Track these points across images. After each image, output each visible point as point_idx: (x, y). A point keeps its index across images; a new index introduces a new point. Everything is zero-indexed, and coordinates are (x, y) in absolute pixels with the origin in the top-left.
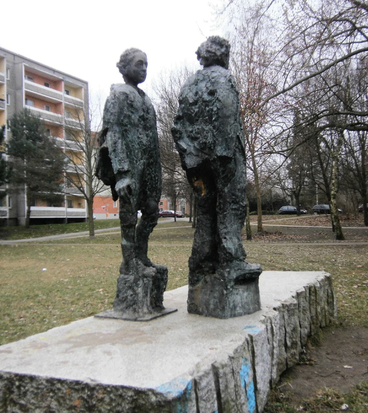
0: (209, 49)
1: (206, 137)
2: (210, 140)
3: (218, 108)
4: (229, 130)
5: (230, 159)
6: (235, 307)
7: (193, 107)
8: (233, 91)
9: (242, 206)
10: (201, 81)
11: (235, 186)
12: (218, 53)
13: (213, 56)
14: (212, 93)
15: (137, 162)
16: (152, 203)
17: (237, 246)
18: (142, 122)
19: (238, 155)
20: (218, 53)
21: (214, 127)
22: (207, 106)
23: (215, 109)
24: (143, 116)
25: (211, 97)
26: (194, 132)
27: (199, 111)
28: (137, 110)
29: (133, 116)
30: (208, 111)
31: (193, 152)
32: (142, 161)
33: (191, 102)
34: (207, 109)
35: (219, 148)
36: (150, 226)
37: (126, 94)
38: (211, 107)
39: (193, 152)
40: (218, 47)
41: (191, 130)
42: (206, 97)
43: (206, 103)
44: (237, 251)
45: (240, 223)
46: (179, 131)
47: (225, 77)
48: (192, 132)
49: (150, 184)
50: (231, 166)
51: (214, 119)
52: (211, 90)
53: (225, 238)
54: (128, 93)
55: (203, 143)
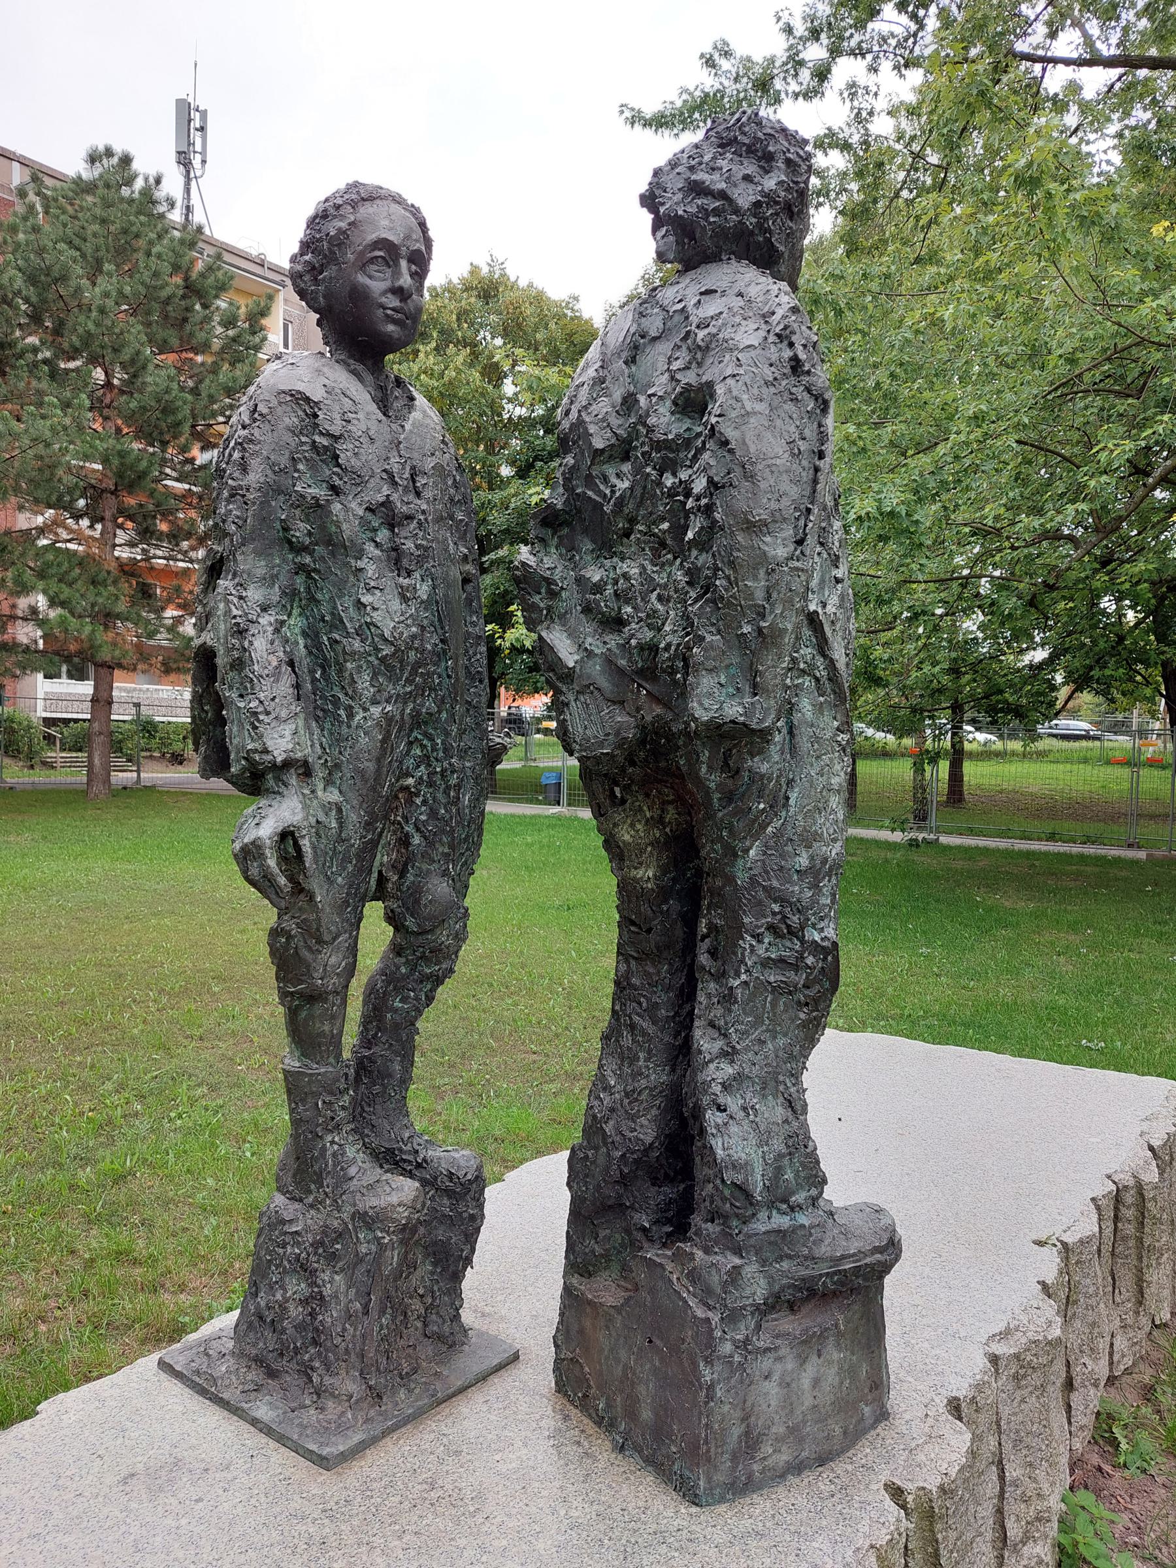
0: (700, 176)
1: (654, 622)
2: (671, 634)
3: (710, 481)
4: (760, 595)
5: (765, 735)
6: (751, 1442)
7: (611, 471)
8: (799, 391)
9: (815, 948)
10: (655, 339)
11: (782, 856)
12: (745, 197)
13: (716, 212)
14: (693, 402)
15: (351, 716)
16: (439, 888)
17: (778, 1145)
18: (383, 535)
19: (806, 706)
20: (745, 197)
21: (693, 575)
22: (670, 466)
23: (699, 485)
24: (387, 503)
25: (687, 423)
26: (609, 590)
27: (632, 488)
28: (360, 481)
29: (336, 507)
30: (672, 493)
31: (604, 683)
32: (376, 711)
33: (598, 444)
34: (669, 481)
35: (706, 683)
36: (424, 978)
37: (307, 400)
38: (684, 475)
39: (604, 683)
40: (750, 168)
41: (596, 578)
42: (666, 422)
43: (671, 454)
44: (779, 1171)
45: (804, 1025)
46: (549, 582)
47: (766, 317)
48: (598, 588)
49: (424, 802)
50: (764, 768)
51: (690, 535)
52: (688, 388)
53: (721, 1109)
54: (317, 394)
55: (641, 647)
